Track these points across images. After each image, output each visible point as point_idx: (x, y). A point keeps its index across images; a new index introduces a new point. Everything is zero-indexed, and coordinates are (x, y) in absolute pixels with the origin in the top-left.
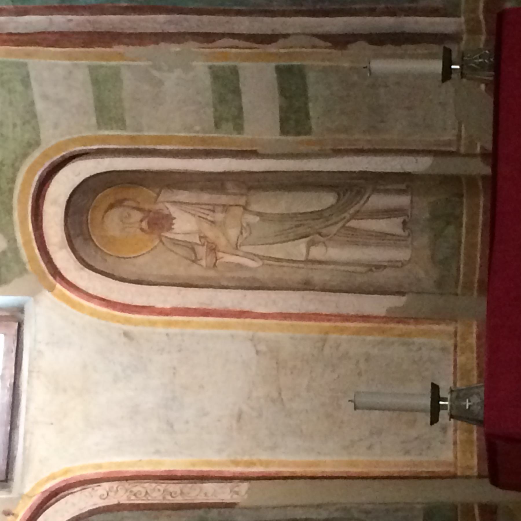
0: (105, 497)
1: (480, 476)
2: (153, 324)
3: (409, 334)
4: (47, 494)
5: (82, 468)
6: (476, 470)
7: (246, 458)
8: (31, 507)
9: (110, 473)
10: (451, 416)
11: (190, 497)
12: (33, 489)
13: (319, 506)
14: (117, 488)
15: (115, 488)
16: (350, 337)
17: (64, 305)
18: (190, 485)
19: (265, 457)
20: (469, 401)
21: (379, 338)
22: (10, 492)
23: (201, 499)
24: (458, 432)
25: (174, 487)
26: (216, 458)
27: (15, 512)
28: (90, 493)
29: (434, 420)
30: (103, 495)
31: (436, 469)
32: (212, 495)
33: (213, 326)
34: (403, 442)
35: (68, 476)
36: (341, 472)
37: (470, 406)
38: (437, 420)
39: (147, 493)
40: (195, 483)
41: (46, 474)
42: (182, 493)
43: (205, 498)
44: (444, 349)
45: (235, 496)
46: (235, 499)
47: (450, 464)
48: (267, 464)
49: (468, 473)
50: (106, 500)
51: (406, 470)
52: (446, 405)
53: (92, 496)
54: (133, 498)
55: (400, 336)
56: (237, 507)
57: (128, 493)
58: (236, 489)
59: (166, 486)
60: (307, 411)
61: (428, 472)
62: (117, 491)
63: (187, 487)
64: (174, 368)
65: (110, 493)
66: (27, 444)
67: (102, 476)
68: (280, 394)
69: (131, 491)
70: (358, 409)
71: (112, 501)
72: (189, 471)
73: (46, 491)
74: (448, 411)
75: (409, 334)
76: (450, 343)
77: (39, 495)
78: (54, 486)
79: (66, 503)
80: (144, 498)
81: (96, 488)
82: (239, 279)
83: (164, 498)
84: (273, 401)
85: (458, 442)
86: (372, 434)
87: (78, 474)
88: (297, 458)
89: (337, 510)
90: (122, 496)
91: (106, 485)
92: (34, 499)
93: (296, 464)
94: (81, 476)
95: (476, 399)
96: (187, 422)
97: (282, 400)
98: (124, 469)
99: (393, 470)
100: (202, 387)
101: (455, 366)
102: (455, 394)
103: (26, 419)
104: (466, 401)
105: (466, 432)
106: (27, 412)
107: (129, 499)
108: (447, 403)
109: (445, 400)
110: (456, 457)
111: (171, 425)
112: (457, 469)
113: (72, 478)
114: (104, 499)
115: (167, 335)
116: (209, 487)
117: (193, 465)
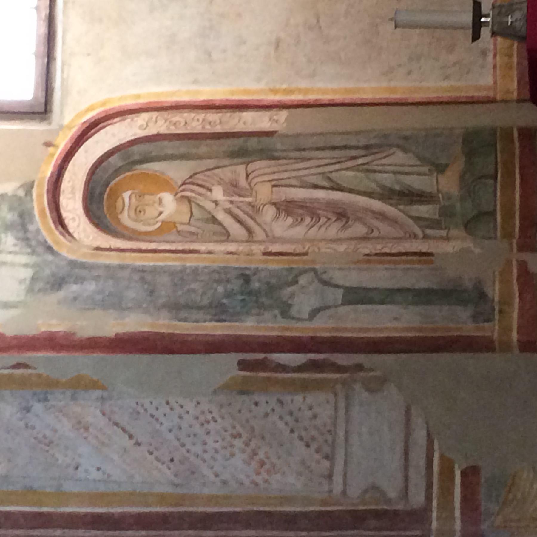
1: (519, 101)
4: (87, 125)
5: (121, 99)
6: (515, 94)
7: (284, 86)
8: (72, 137)
9: (150, 103)
10: (494, 34)
12: (73, 120)
13: (358, 133)
14: (157, 118)
15: (154, 119)
18: (228, 114)
19: (303, 84)
20: (511, 17)
22: (50, 124)
23: (240, 127)
24: (498, 58)
25: (213, 116)
26: (254, 86)
27: (56, 143)
29: (476, 36)
31: (476, 94)
32: (251, 124)
35: (108, 107)
36: (380, 99)
37: (512, 22)
38: (479, 37)
39: (186, 123)
40: (234, 112)
41: (83, 107)
46: (274, 127)
47: (488, 88)
48: (307, 91)
49: (509, 97)
50: (147, 131)
51: (446, 96)
52: (488, 22)
54: (172, 127)
56: (277, 134)
58: (275, 117)
59: (205, 116)
61: (467, 97)
62: (156, 121)
63: (227, 115)
65: (149, 124)
66: (65, 76)
67: (140, 106)
68: (318, 21)
69: (170, 122)
70: (399, 27)
71: (152, 131)
72: (227, 100)
73: (84, 122)
74: (490, 27)
77: (80, 126)
78: (93, 117)
81: (135, 119)
82: (61, 233)
83: (203, 128)
84: (311, 28)
85: (498, 66)
86: (411, 59)
87: (116, 105)
88: (334, 85)
89: (375, 137)
90: (161, 126)
91: (145, 116)
92: (74, 130)
93: (334, 91)
94: (120, 106)
95: (518, 15)
97: (320, 27)
98: (163, 99)
99: (433, 96)
100: (239, 15)
102: (496, 11)
103: (63, 51)
104: (508, 18)
105: (506, 56)
106: (63, 43)
108: (489, 20)
109: (486, 16)
110: (495, 82)
113: (110, 109)
116: (248, 116)
117: (233, 93)
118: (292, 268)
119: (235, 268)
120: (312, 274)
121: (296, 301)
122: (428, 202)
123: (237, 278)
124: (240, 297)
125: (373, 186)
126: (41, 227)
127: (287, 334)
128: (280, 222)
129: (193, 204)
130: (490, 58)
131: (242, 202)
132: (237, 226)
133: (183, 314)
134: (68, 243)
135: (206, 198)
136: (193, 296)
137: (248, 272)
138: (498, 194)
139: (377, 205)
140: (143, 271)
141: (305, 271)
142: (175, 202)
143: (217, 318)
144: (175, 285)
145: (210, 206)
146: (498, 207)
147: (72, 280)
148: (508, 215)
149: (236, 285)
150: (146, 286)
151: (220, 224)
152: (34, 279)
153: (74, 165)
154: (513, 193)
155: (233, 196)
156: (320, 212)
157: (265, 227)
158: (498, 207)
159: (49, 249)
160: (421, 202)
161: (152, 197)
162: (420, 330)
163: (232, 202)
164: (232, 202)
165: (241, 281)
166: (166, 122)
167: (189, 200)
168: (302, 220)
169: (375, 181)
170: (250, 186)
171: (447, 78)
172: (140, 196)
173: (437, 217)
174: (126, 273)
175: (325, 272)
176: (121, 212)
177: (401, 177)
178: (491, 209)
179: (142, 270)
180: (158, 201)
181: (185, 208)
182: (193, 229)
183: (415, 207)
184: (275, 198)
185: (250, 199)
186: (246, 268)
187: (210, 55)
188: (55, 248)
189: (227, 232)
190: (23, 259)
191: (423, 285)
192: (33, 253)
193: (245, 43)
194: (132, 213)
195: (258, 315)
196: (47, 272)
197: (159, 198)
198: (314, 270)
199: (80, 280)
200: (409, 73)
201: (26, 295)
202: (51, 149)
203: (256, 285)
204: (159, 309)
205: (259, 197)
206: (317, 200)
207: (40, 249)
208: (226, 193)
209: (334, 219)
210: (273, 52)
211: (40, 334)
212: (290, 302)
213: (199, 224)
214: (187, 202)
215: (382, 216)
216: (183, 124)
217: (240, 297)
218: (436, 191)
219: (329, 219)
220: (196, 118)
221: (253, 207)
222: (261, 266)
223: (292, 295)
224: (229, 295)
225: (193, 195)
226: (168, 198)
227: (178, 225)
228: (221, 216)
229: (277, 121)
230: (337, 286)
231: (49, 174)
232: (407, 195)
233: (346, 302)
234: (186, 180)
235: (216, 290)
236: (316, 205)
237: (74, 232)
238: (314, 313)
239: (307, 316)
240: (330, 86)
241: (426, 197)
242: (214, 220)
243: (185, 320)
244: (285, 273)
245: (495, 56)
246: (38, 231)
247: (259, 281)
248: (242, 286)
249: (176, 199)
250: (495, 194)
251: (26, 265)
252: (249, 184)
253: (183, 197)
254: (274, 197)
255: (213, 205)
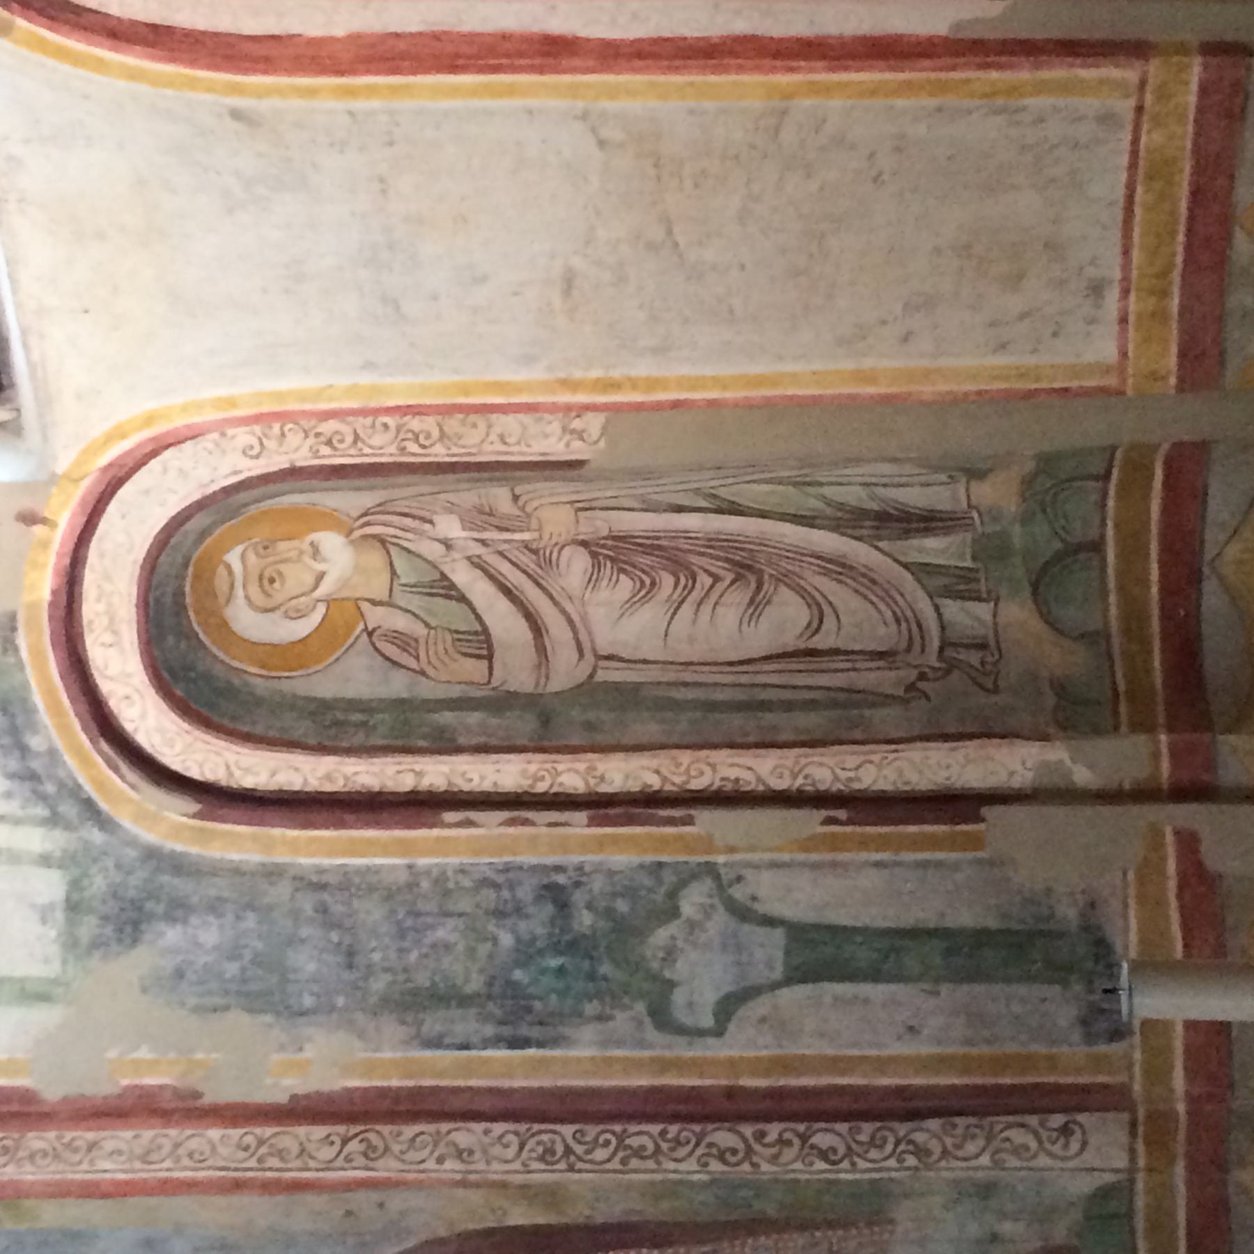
0: (254, 452)
2: (311, 92)
3: (1013, 91)
5: (184, 409)
7: (596, 373)
11: (464, 447)
12: (78, 463)
16: (850, 102)
17: (51, 62)
19: (643, 369)
21: (932, 102)
24: (1132, 297)
28: (217, 445)
30: (252, 447)
33: (474, 92)
34: (993, 324)
41: (99, 429)
42: (443, 436)
43: (503, 448)
44: (1107, 119)
45: (577, 444)
46: (578, 450)
47: (1107, 370)
48: (653, 384)
50: (262, 461)
53: (224, 452)
54: (325, 450)
55: (985, 96)
56: (586, 467)
57: (311, 440)
60: (743, 267)
62: (283, 435)
64: (382, 180)
66: (35, 356)
68: (670, 232)
75: (1013, 91)
76: (1125, 107)
79: (165, 470)
80: (352, 451)
84: (652, 247)
85: (1132, 318)
90: (297, 449)
92: (85, 484)
96: (435, 298)
97: (676, 245)
101: (1134, 153)
107: (316, 454)
110: (1124, 354)
111: (393, 303)
112: (1124, 381)
114: (257, 457)
115: (351, 114)
118: (660, 865)
119: (534, 869)
120: (708, 884)
121: (680, 970)
122: (947, 531)
123: (539, 899)
124: (554, 962)
125: (814, 503)
126: (59, 744)
127: (672, 1080)
128: (604, 593)
129: (394, 551)
130: (1112, 297)
131: (506, 541)
132: (503, 604)
133: (433, 1023)
134: (132, 794)
135: (421, 533)
136: (446, 962)
137: (561, 879)
138: (1111, 503)
139: (826, 541)
140: (323, 887)
141: (694, 876)
142: (350, 548)
143: (506, 1031)
144: (402, 934)
145: (432, 550)
146: (1110, 532)
147: (160, 909)
148: (1132, 549)
149: (537, 923)
150: (335, 936)
151: (462, 599)
152: (74, 907)
153: (102, 556)
154: (1146, 497)
155: (485, 529)
156: (694, 559)
157: (569, 608)
158: (1110, 532)
159: (89, 806)
160: (927, 531)
161: (295, 543)
162: (966, 1065)
163: (483, 542)
164: (483, 542)
165: (549, 909)
166: (306, 436)
167: (382, 541)
168: (653, 584)
169: (823, 498)
170: (525, 512)
171: (1003, 347)
172: (266, 548)
173: (968, 563)
174: (281, 892)
175: (739, 879)
176: (228, 601)
177: (881, 491)
178: (1093, 534)
179: (314, 884)
180: (310, 550)
181: (375, 558)
182: (401, 622)
183: (915, 542)
184: (585, 532)
185: (526, 536)
186: (559, 869)
187: (397, 308)
188: (103, 805)
189: (485, 631)
190: (35, 840)
191: (965, 918)
192: (54, 820)
193: (484, 279)
194: (254, 590)
195: (601, 1018)
196: (98, 884)
197: (312, 544)
198: (711, 870)
199: (178, 910)
200: (906, 339)
201: (64, 962)
202: (38, 530)
203: (585, 920)
204: (375, 1014)
205: (548, 529)
206: (686, 535)
207: (68, 809)
208: (466, 524)
209: (729, 577)
210: (557, 301)
211: (120, 1096)
212: (667, 974)
213: (415, 603)
214: (378, 544)
215: (839, 568)
216: (349, 439)
217: (554, 962)
218: (964, 505)
219: (716, 579)
220: (378, 424)
221: (535, 552)
222: (590, 859)
223: (670, 955)
224: (526, 953)
225: (392, 531)
226: (331, 542)
227: (365, 606)
228: (463, 576)
229: (580, 435)
230: (770, 921)
231: (46, 595)
232: (899, 520)
233: (798, 975)
234: (369, 509)
235: (495, 940)
236: (682, 544)
237: (136, 730)
238: (727, 1008)
239: (708, 1021)
240: (708, 371)
241: (941, 520)
242: (447, 589)
243: (435, 1043)
244: (647, 881)
245: (1125, 292)
246: (52, 753)
247: (589, 906)
248: (552, 922)
249: (352, 542)
250: (1103, 505)
251: (45, 860)
252: (523, 509)
253: (365, 537)
254: (582, 529)
255: (440, 548)
